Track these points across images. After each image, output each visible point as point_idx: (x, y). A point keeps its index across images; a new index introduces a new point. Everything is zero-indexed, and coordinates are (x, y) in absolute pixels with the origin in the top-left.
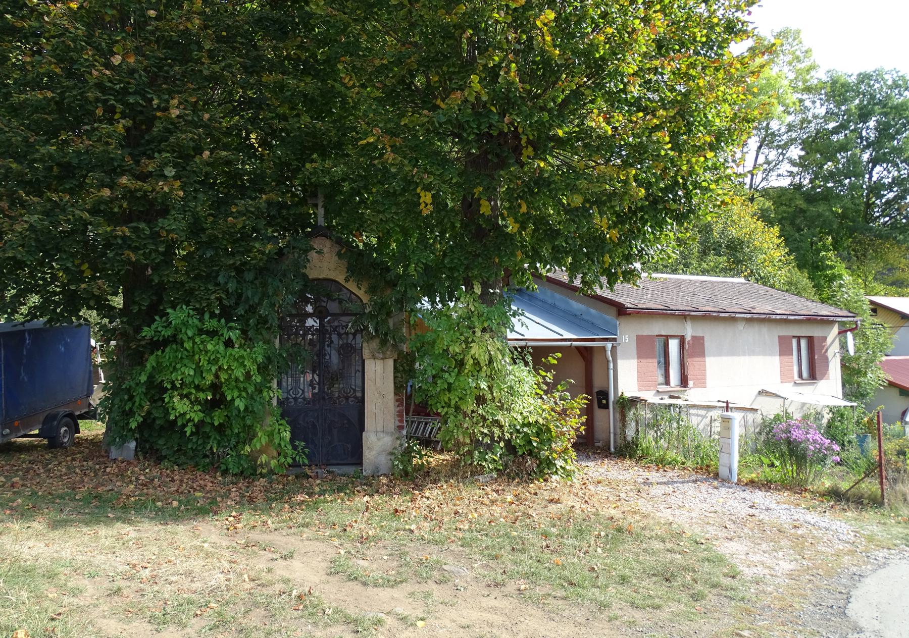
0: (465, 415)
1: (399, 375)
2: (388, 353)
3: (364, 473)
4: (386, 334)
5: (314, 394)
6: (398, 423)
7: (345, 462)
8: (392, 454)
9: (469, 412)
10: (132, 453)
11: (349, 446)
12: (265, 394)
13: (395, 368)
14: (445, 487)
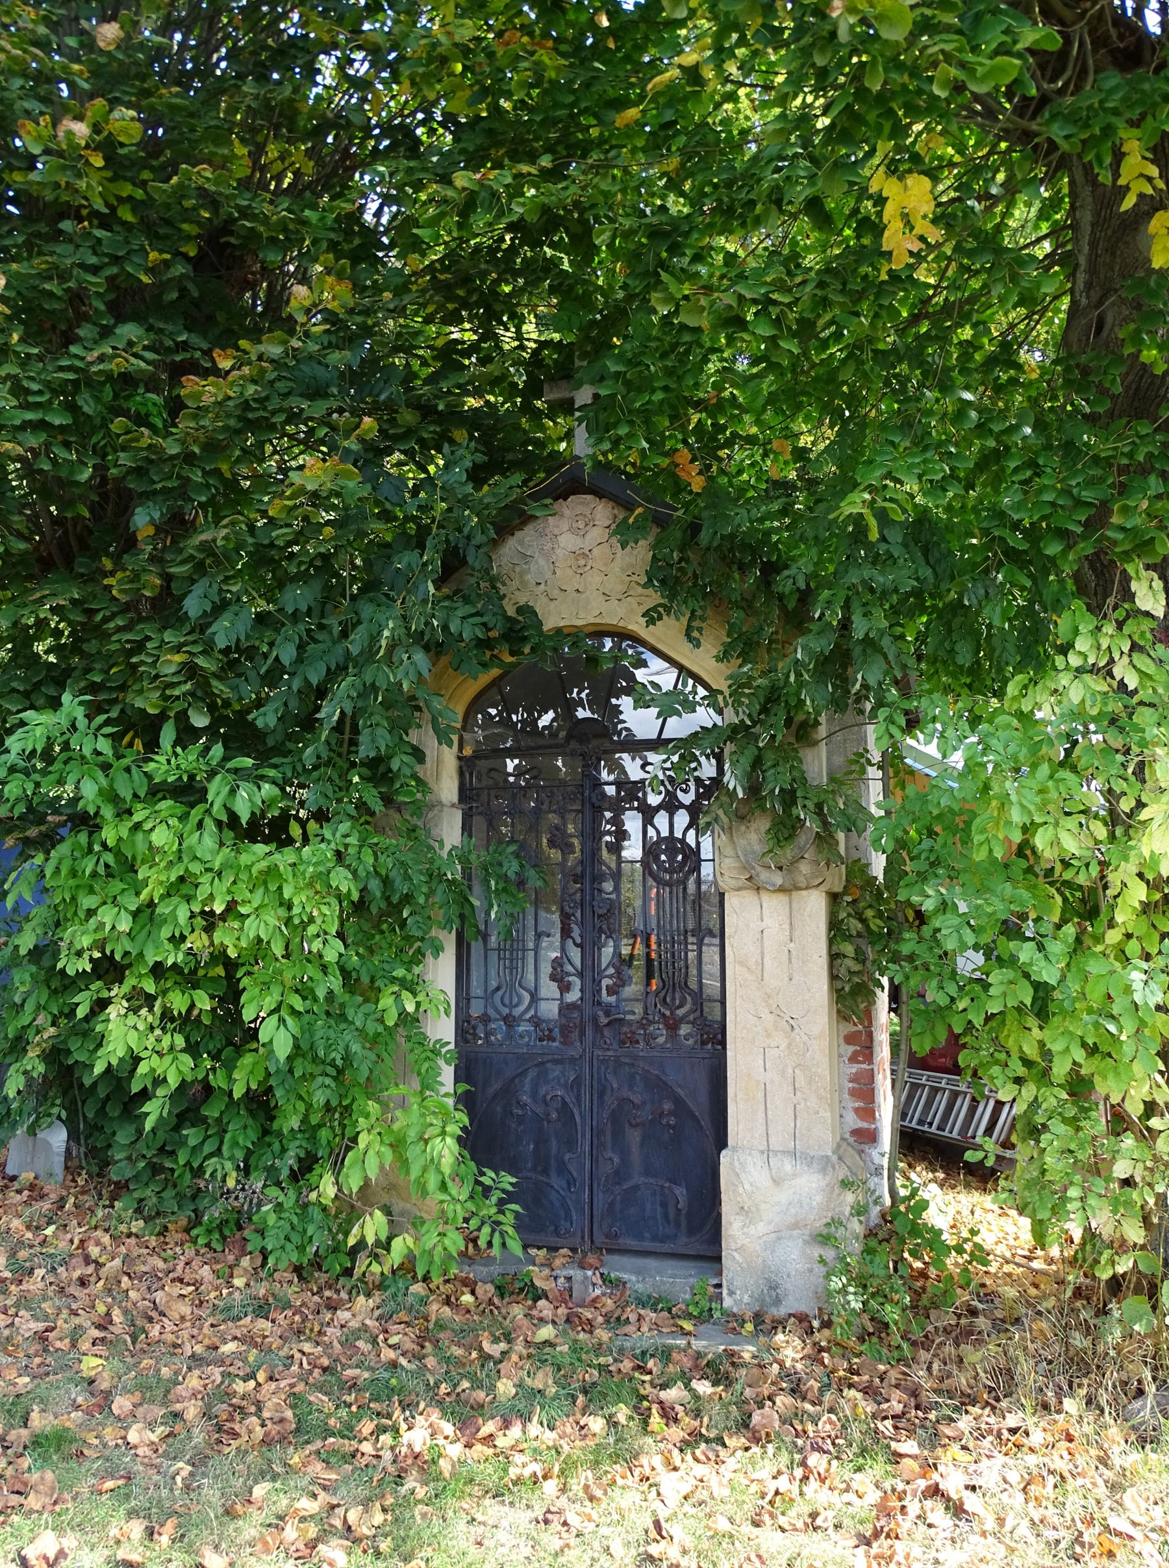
0: (1119, 1121)
1: (848, 949)
2: (804, 868)
3: (728, 1302)
4: (789, 798)
5: (565, 1009)
6: (853, 1121)
7: (667, 1247)
8: (824, 1239)
9: (1134, 1109)
10: (58, 1163)
11: (680, 1192)
12: (387, 1001)
13: (835, 928)
14: (1037, 1438)
